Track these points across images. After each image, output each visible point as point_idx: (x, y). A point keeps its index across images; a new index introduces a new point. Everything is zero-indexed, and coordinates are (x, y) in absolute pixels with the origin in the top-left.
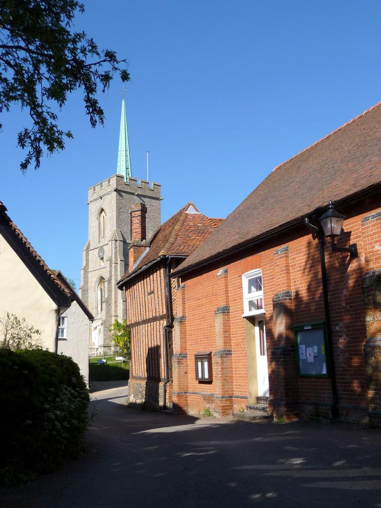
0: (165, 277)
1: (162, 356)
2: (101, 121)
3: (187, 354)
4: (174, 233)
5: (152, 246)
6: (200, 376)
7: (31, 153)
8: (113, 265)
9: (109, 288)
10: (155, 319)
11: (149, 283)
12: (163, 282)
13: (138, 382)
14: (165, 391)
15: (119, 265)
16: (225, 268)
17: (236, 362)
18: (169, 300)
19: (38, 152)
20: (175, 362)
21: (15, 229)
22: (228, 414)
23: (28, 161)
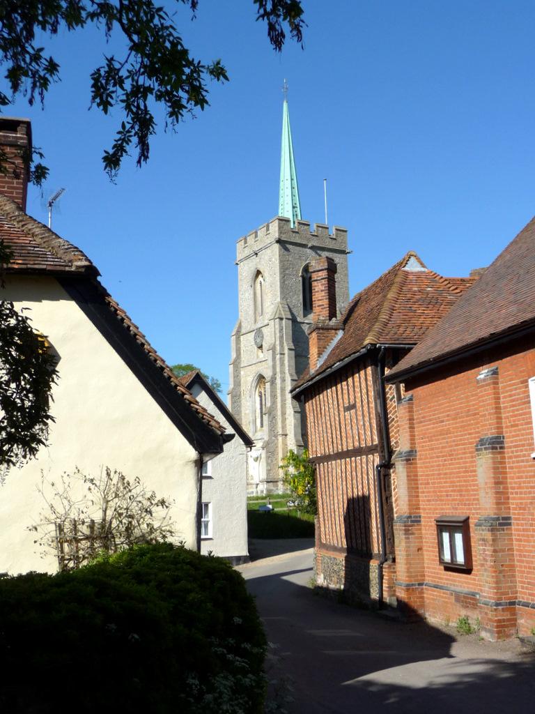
0: (375, 382)
1: (373, 515)
2: (295, 32)
3: (420, 517)
4: (386, 305)
5: (347, 328)
6: (447, 557)
7: (128, 126)
8: (278, 357)
9: (272, 392)
10: (358, 452)
11: (345, 391)
12: (371, 389)
13: (332, 554)
14: (381, 577)
15: (286, 356)
16: (493, 366)
17: (520, 540)
18: (382, 420)
19: (144, 123)
20: (400, 530)
21: (116, 310)
22: (508, 636)
23: (120, 149)
